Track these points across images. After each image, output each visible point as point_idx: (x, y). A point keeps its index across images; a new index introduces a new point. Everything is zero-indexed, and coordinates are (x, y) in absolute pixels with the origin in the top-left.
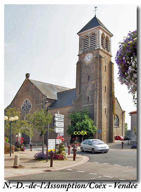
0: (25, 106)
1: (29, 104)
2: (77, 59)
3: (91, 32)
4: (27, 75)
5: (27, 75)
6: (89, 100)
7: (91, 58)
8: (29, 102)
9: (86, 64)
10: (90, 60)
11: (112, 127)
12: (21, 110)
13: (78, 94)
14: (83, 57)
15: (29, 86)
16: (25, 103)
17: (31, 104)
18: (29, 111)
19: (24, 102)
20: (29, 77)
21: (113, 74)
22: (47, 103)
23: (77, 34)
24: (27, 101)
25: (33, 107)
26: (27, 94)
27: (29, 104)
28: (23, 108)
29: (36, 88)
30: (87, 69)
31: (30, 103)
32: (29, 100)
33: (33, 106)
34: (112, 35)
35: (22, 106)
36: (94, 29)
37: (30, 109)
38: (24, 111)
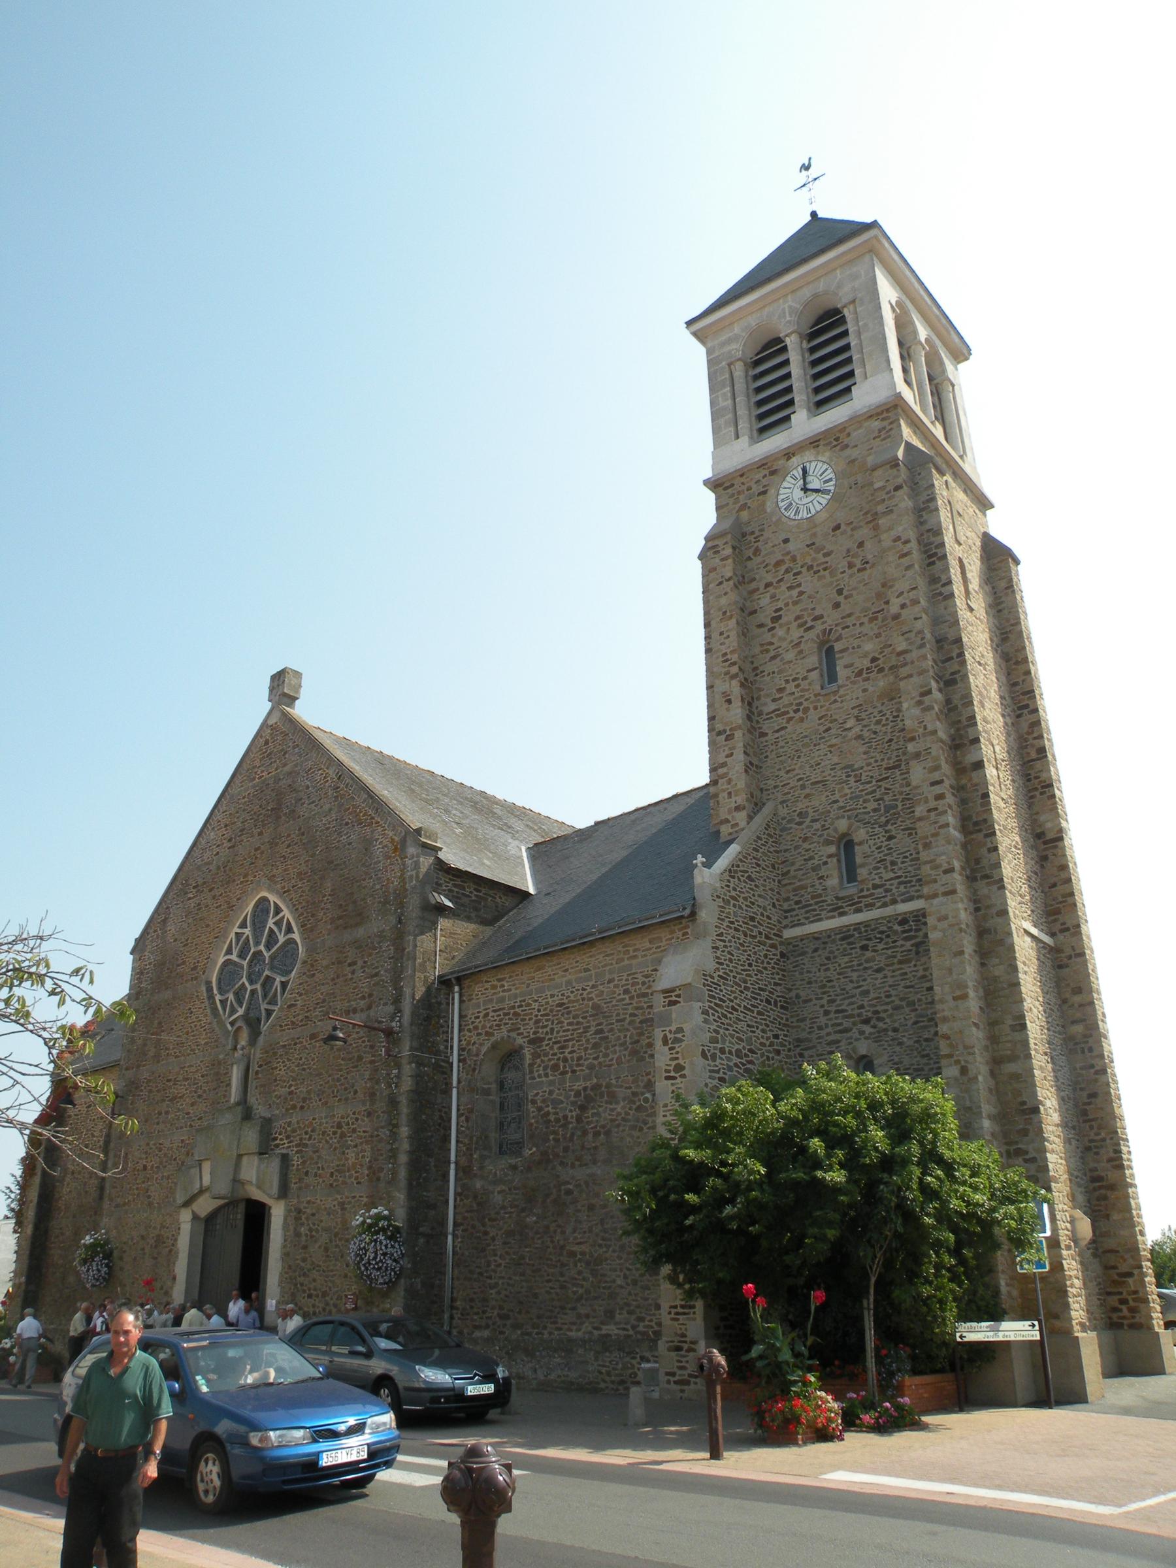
0: (242, 955)
1: (282, 939)
2: (702, 514)
3: (806, 293)
4: (283, 687)
5: (283, 687)
6: (862, 873)
7: (830, 486)
8: (286, 913)
9: (786, 541)
10: (824, 499)
11: (1112, 1176)
12: (211, 997)
13: (738, 809)
14: (756, 489)
15: (287, 769)
16: (247, 931)
17: (296, 936)
18: (273, 1002)
19: (243, 925)
20: (292, 700)
21: (1029, 638)
22: (441, 909)
23: (689, 323)
24: (262, 907)
25: (310, 965)
26: (273, 844)
27: (282, 939)
28: (229, 972)
29: (343, 773)
30: (808, 582)
31: (289, 930)
32: (283, 893)
33: (311, 950)
34: (961, 353)
35: (221, 960)
36: (828, 269)
37: (284, 985)
38: (233, 1011)
